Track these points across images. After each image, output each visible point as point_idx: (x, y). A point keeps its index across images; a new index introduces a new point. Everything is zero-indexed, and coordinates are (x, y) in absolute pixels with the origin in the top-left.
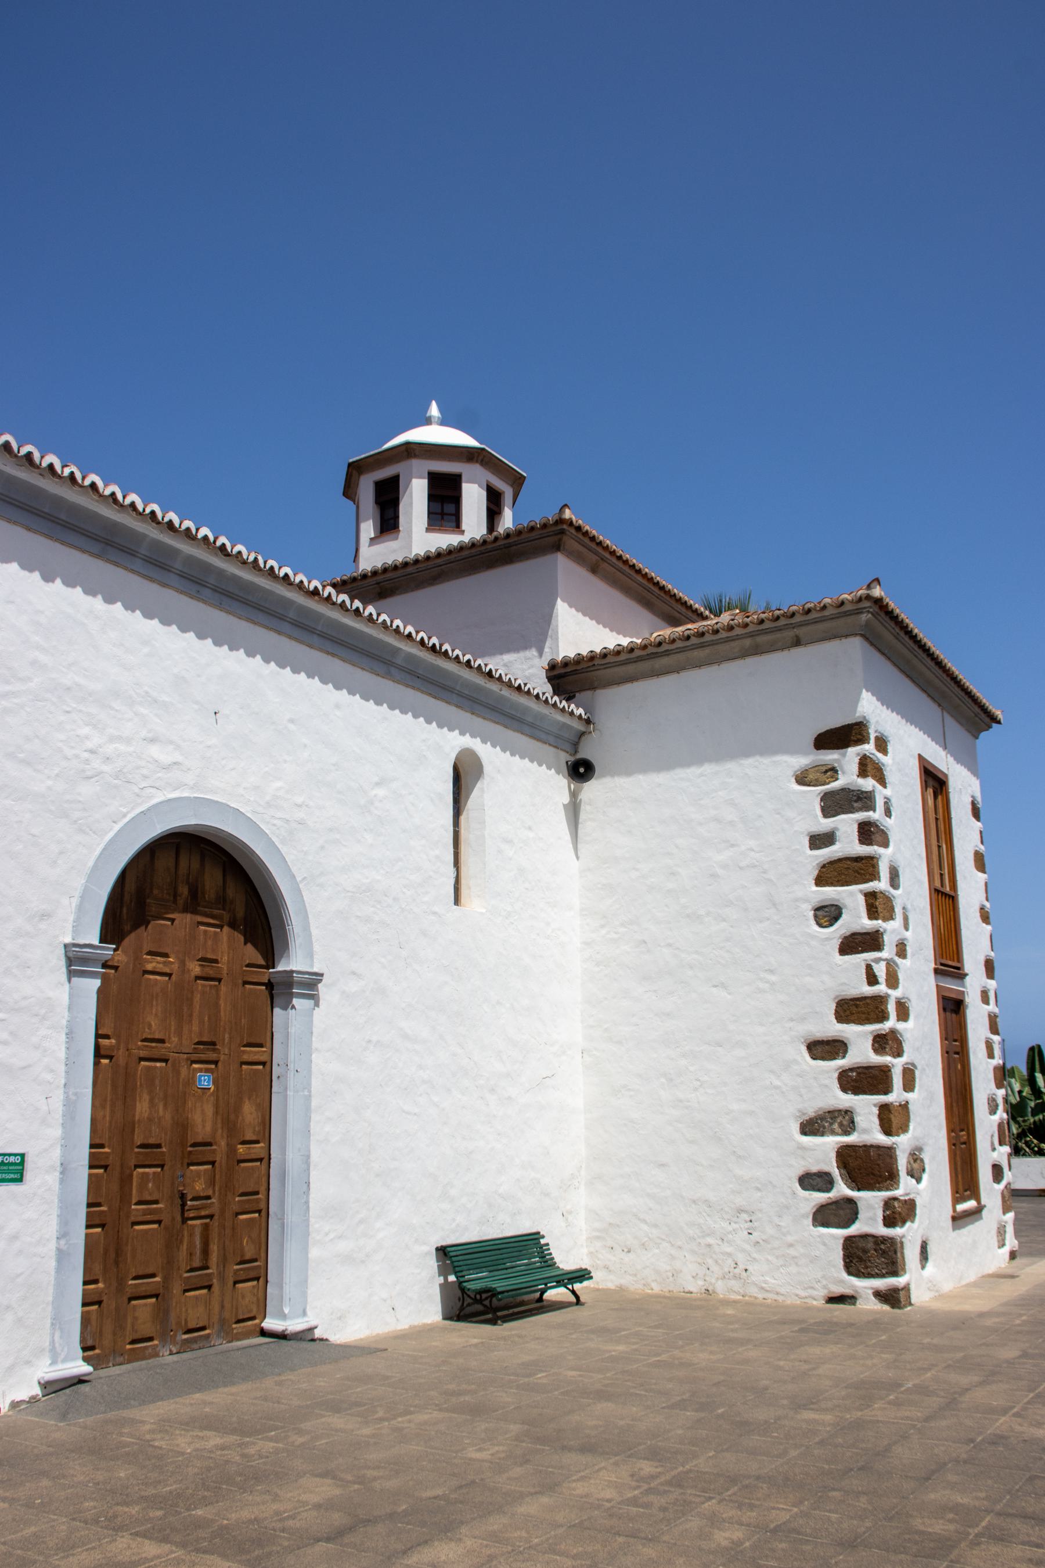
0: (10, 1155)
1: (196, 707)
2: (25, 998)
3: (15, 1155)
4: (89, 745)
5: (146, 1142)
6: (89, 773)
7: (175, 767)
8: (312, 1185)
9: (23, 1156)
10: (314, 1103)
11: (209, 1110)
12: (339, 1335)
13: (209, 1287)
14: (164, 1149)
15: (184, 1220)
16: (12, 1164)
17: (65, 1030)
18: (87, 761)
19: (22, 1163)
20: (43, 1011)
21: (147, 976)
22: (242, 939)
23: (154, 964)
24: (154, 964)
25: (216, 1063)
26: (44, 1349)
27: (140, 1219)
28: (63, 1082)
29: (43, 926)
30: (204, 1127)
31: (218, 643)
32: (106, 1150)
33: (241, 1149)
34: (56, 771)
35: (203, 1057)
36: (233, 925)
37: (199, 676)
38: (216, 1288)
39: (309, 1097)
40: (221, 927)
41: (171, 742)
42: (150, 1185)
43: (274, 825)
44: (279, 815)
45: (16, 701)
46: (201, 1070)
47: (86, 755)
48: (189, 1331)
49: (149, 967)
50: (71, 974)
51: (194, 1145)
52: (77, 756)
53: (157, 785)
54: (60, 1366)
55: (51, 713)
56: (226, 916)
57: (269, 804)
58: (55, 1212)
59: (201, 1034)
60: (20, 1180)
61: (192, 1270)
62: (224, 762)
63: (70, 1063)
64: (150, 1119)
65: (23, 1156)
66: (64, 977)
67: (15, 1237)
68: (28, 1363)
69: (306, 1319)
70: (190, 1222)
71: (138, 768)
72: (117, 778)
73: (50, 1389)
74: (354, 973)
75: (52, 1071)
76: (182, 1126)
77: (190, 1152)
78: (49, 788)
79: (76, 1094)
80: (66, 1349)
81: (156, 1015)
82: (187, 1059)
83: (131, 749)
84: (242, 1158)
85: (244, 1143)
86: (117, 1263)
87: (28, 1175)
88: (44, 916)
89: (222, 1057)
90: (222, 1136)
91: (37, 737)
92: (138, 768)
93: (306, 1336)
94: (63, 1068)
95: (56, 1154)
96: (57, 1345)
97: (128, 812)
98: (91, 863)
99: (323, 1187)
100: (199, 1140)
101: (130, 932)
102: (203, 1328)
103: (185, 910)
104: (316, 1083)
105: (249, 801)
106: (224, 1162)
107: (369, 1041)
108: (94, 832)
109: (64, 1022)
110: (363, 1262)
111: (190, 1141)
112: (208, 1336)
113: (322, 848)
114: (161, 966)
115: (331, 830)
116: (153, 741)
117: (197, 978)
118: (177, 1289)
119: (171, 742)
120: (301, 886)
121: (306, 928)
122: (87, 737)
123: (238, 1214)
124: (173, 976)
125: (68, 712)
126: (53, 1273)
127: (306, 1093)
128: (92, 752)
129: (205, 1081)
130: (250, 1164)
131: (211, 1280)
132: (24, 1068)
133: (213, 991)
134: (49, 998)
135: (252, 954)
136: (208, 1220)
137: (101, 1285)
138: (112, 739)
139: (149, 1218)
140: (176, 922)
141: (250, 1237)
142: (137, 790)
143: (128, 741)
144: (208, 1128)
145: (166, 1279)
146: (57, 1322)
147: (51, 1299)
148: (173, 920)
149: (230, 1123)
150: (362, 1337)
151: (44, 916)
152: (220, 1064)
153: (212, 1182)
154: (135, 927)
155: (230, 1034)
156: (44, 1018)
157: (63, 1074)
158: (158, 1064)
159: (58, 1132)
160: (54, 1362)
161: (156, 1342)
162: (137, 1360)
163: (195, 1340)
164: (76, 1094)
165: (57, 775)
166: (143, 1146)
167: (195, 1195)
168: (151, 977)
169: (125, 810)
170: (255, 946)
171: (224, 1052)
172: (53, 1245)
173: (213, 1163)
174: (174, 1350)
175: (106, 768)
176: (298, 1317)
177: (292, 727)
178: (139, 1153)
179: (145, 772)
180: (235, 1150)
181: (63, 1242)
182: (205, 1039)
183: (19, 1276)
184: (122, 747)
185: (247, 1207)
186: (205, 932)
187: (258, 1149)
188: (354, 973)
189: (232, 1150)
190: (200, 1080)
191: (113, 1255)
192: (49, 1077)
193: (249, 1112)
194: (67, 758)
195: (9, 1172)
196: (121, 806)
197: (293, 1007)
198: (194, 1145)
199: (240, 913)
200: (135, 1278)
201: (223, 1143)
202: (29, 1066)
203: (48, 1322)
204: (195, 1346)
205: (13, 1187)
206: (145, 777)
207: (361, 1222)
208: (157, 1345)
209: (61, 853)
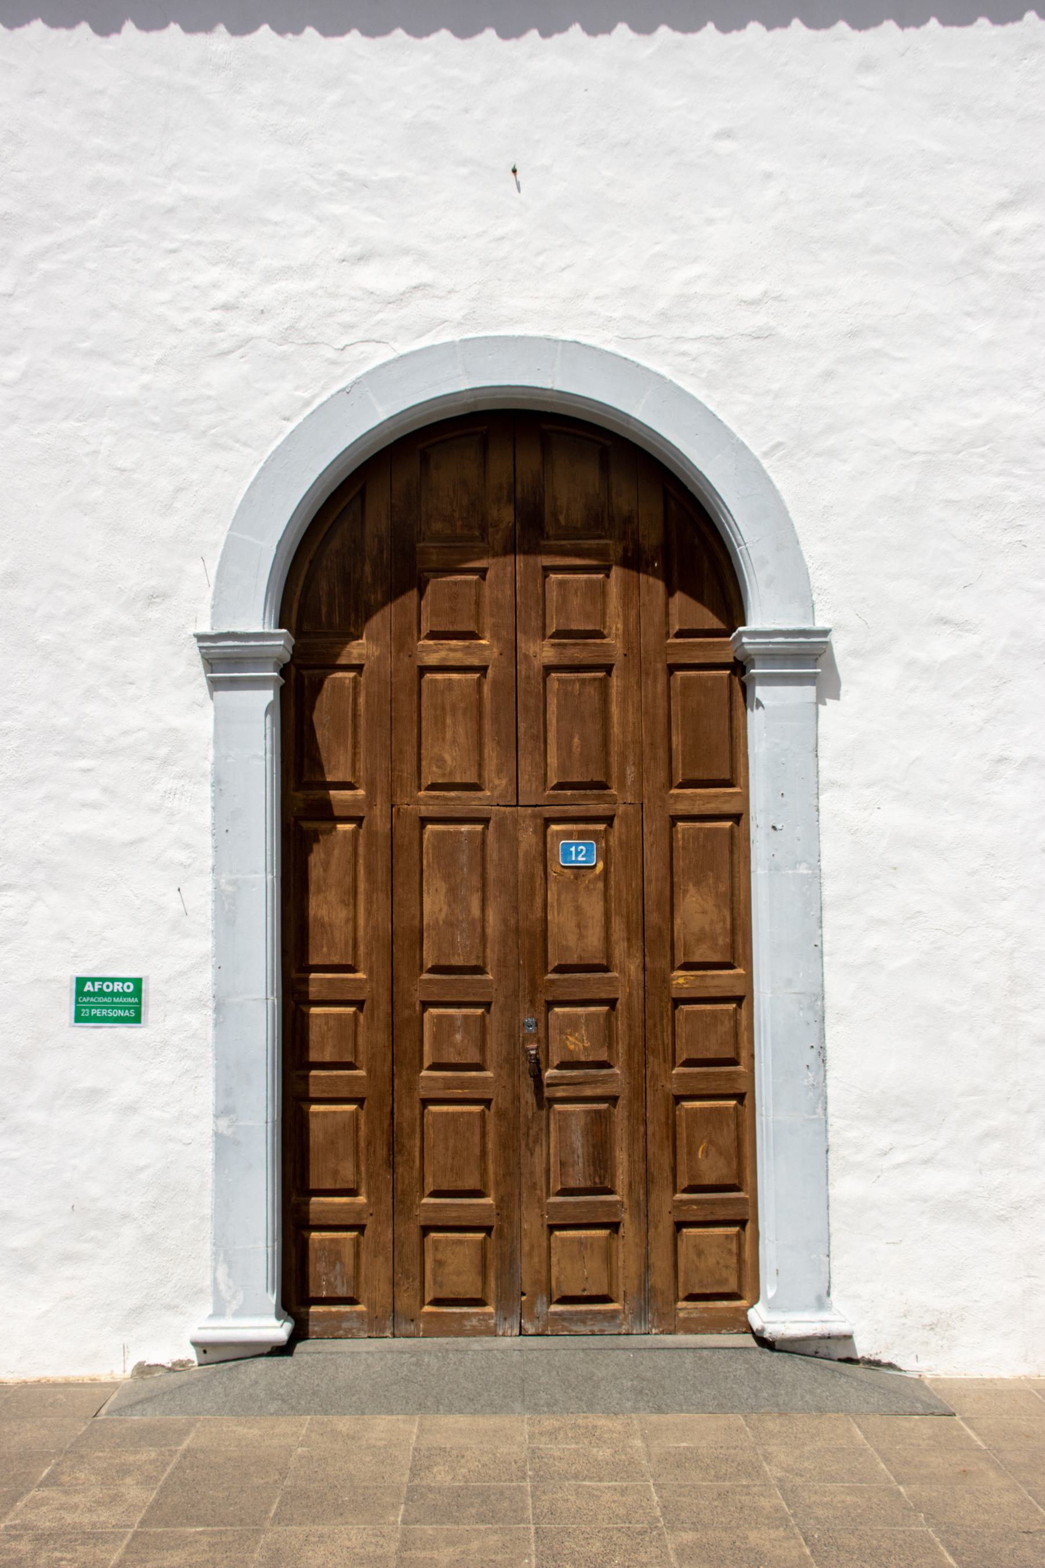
0: (113, 980)
1: (464, 171)
2: (125, 733)
3: (123, 980)
4: (220, 297)
5: (444, 962)
6: (224, 346)
7: (419, 294)
8: (830, 1054)
9: (138, 982)
10: (830, 890)
11: (594, 908)
12: (924, 1361)
13: (614, 1227)
14: (490, 977)
15: (544, 1103)
16: (118, 994)
17: (210, 779)
18: (218, 327)
19: (138, 992)
20: (163, 752)
21: (428, 676)
22: (660, 585)
23: (443, 654)
24: (443, 654)
25: (609, 820)
26: (201, 1291)
27: (441, 1094)
28: (210, 862)
29: (154, 613)
30: (581, 937)
31: (508, 32)
32: (360, 975)
33: (681, 979)
34: (158, 354)
35: (573, 810)
36: (634, 562)
37: (466, 111)
38: (628, 1229)
39: (816, 877)
40: (606, 570)
41: (406, 251)
42: (458, 1037)
43: (684, 354)
44: (694, 331)
45: (65, 257)
46: (569, 835)
47: (216, 316)
48: (565, 1300)
49: (432, 659)
50: (215, 685)
51: (561, 969)
52: (196, 322)
53: (376, 336)
54: (230, 1322)
55: (138, 261)
56: (614, 547)
57: (665, 316)
58: (208, 1075)
59: (562, 768)
60: (137, 1019)
61: (565, 1192)
62: (542, 259)
63: (223, 831)
64: (450, 924)
65: (138, 982)
66: (206, 690)
67: (130, 1109)
68: (170, 1307)
69: (824, 1315)
70: (558, 1107)
71: (331, 314)
72: (284, 340)
73: (212, 1355)
74: (944, 621)
75: (187, 846)
76: (533, 940)
77: (552, 982)
78: (146, 387)
79: (234, 883)
80: (240, 1296)
81: (454, 741)
82: (534, 816)
83: (311, 285)
84: (684, 995)
85: (688, 966)
86: (392, 1166)
87: (151, 1011)
88: (154, 598)
89: (621, 809)
90: (629, 955)
91: (114, 307)
92: (331, 314)
93: (829, 1352)
94: (208, 841)
95: (205, 980)
96: (222, 1287)
97: (314, 397)
98: (239, 499)
99: (858, 1061)
100: (573, 960)
101: (384, 604)
102: (605, 1299)
103: (510, 548)
104: (832, 852)
105: (610, 319)
106: (637, 1003)
107: (1002, 760)
108: (245, 444)
109: (208, 766)
110: (1003, 1219)
111: (554, 963)
112: (613, 1315)
113: (828, 375)
114: (459, 655)
115: (853, 334)
116: (362, 258)
117: (548, 669)
118: (531, 1222)
119: (406, 251)
120: (765, 464)
121: (788, 541)
122: (215, 286)
123: (678, 1099)
124: (490, 672)
125: (173, 251)
126: (209, 1169)
127: (803, 870)
128: (226, 307)
129: (578, 852)
130: (709, 1007)
131: (616, 1214)
132: (132, 843)
133: (591, 691)
134: (175, 730)
135: (685, 610)
136: (604, 1106)
137: (362, 1199)
138: (270, 276)
139: (458, 1093)
140: (489, 575)
141: (711, 1142)
142: (331, 354)
143: (306, 271)
144: (594, 938)
145: (502, 1203)
146: (223, 1249)
147: (208, 1211)
148: (482, 572)
149: (652, 932)
150: (1006, 1376)
151: (154, 598)
152: (616, 822)
153: (609, 1039)
154: (394, 593)
155: (639, 764)
156: (166, 762)
157: (210, 851)
158: (464, 828)
159: (207, 945)
160: (218, 1312)
161: (490, 1309)
162: (446, 1334)
163: (582, 1318)
164: (234, 883)
165: (159, 362)
166: (436, 970)
167: (568, 1058)
168: (439, 676)
169: (307, 395)
170: (696, 595)
171: (621, 799)
172: (206, 1126)
173: (612, 1003)
174: (531, 1330)
175: (256, 330)
176: (805, 1308)
177: (726, 146)
178: (430, 981)
179: (346, 318)
180: (666, 981)
181: (223, 1123)
182: (575, 778)
183: (142, 1169)
184: (291, 286)
185: (702, 1087)
186: (561, 584)
187: (721, 980)
188: (944, 621)
189: (654, 982)
190: (567, 853)
191: (382, 1152)
192: (182, 856)
193: (696, 911)
194: (177, 330)
195: (114, 1006)
196: (296, 389)
197: (759, 704)
198: (561, 969)
199: (651, 536)
200: (435, 1194)
201: (633, 967)
202: (141, 840)
203: (208, 1248)
204: (581, 1328)
205: (123, 1031)
206: (349, 327)
207: (989, 1135)
208: (490, 1315)
209: (179, 490)
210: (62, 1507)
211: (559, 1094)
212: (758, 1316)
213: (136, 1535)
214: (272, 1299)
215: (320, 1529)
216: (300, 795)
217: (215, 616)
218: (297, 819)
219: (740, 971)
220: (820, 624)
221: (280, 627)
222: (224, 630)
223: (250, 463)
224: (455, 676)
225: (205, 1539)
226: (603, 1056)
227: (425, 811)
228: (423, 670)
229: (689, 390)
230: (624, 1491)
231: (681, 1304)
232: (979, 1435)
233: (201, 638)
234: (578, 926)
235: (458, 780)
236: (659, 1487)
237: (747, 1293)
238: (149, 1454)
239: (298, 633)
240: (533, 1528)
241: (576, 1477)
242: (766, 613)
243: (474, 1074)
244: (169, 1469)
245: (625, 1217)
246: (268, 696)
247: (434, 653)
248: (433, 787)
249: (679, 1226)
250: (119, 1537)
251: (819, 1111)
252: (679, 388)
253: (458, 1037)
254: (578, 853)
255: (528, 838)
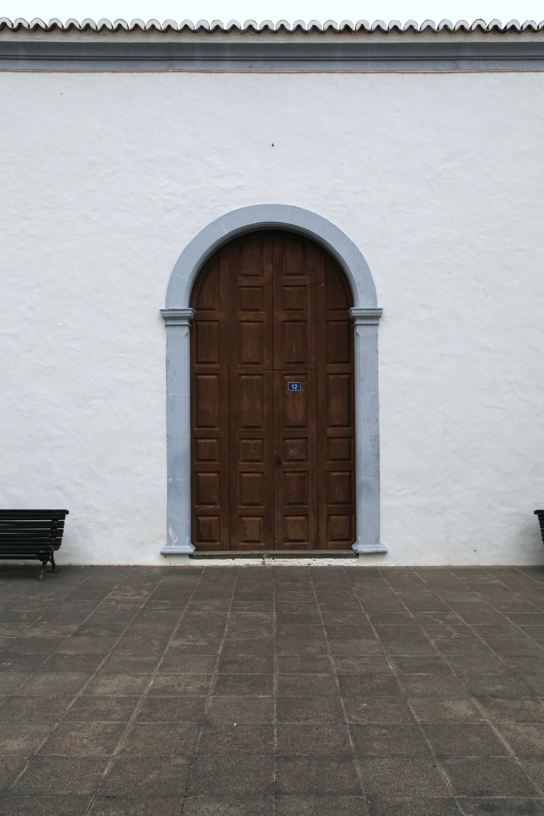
32: (218, 429)
38: (312, 517)
49: (243, 318)
79: (174, 397)
80: (177, 538)
96: (171, 535)
112: (306, 546)
127: (373, 393)
150: (439, 565)
210: (123, 595)
211: (288, 470)
212: (354, 547)
213: (147, 602)
214: (188, 539)
215: (206, 602)
216: (196, 365)
217: (167, 303)
218: (196, 374)
219: (351, 428)
220: (379, 306)
221: (190, 307)
222: (170, 308)
223: (180, 249)
224: (251, 324)
225: (170, 604)
226: (303, 457)
227: (240, 372)
228: (240, 321)
229: (334, 224)
230: (305, 594)
231: (329, 543)
232: (425, 579)
233: (161, 310)
234: (296, 412)
235: (252, 361)
236: (316, 593)
237: (353, 539)
238: (149, 584)
239: (197, 309)
240: (275, 602)
241: (290, 590)
242: (362, 303)
243: (258, 463)
244: (156, 588)
245: (311, 513)
246: (186, 330)
247: (244, 316)
248: (331, 309)
249: (329, 515)
250: (142, 603)
251: (377, 476)
252: (331, 223)
253: (252, 451)
254: (294, 387)
255: (277, 382)
